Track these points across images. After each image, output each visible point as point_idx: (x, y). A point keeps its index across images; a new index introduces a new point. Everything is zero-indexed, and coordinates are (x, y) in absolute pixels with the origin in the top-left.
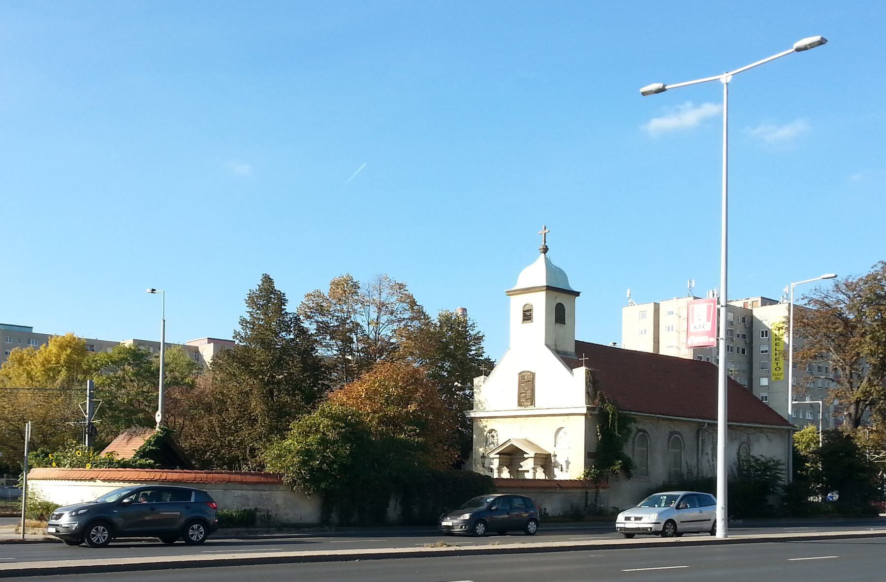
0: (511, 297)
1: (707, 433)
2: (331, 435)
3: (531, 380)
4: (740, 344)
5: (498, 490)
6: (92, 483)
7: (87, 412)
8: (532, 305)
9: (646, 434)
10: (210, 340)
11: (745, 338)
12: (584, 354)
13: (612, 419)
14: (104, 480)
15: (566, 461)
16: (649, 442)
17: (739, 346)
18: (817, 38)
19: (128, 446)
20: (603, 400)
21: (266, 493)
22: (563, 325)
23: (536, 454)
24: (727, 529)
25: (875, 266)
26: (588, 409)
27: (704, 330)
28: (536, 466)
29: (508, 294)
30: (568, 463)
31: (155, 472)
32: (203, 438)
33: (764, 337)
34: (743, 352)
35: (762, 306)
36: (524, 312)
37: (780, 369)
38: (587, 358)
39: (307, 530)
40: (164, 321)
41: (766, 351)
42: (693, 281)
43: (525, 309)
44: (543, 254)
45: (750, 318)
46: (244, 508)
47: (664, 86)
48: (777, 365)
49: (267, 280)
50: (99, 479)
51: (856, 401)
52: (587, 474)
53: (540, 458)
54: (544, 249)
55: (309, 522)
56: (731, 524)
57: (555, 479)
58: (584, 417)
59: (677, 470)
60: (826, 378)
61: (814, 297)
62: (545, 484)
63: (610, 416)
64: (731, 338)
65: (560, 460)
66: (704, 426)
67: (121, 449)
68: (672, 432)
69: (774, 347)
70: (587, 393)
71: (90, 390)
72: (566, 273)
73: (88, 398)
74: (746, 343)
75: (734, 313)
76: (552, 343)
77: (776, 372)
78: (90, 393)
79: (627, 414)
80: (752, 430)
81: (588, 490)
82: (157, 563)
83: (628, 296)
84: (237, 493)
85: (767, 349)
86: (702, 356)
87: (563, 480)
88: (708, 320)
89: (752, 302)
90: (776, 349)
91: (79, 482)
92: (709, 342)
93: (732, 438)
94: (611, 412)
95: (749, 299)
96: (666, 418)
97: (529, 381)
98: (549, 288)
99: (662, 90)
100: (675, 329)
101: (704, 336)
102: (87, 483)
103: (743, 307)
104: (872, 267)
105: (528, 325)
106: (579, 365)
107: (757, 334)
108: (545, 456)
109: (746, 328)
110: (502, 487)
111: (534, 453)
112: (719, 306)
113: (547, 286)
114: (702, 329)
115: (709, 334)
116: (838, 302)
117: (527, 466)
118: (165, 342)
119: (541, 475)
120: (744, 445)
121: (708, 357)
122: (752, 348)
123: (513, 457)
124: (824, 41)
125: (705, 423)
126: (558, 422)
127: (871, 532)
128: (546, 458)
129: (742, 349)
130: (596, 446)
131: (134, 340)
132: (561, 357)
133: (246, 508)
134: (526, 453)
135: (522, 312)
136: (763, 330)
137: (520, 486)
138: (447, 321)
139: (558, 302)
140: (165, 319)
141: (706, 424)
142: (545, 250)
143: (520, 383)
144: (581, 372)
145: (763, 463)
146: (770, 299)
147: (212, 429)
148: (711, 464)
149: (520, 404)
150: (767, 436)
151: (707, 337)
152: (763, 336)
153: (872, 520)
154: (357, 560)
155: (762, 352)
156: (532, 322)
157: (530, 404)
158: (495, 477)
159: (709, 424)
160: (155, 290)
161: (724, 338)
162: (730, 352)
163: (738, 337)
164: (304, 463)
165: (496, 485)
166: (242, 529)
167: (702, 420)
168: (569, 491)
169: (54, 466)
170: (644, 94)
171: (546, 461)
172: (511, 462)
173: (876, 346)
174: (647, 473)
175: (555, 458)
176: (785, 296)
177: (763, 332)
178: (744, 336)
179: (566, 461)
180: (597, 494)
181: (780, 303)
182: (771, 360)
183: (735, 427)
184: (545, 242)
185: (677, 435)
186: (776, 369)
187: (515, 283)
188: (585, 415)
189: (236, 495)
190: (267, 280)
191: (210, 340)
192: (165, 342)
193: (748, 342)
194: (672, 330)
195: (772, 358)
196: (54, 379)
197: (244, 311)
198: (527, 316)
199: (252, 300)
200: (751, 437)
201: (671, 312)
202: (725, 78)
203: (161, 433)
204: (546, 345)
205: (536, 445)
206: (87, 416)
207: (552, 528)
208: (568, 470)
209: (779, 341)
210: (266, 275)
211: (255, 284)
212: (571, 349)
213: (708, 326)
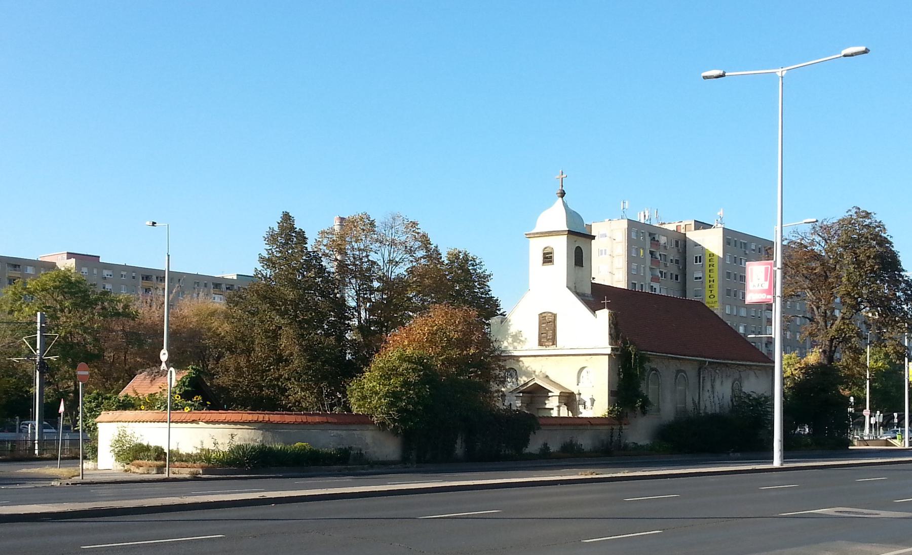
0: (529, 239)
1: (707, 371)
2: (413, 378)
3: (553, 320)
5: (541, 427)
6: (194, 425)
7: (38, 347)
8: (552, 248)
9: (657, 373)
11: (678, 264)
12: (606, 297)
13: (634, 359)
14: (207, 422)
15: (590, 399)
16: (660, 380)
17: (672, 272)
18: (863, 48)
19: (153, 386)
20: (625, 343)
21: (358, 432)
22: (581, 268)
23: (561, 393)
24: (783, 460)
25: (850, 210)
26: (612, 349)
27: (762, 288)
28: (560, 404)
29: (528, 236)
30: (593, 401)
31: (257, 413)
32: (231, 378)
33: (698, 263)
34: (677, 279)
35: (695, 229)
36: (544, 254)
37: (714, 296)
38: (609, 301)
39: (393, 466)
40: (169, 256)
41: (700, 278)
42: (627, 202)
43: (545, 252)
44: (561, 199)
45: (683, 243)
46: (339, 447)
47: (724, 73)
48: (711, 292)
49: (287, 217)
50: (202, 421)
51: (831, 338)
52: (610, 412)
53: (564, 396)
54: (561, 193)
55: (393, 460)
56: (785, 457)
57: (580, 416)
58: (607, 356)
60: (803, 317)
61: (794, 239)
62: (570, 422)
63: (633, 356)
64: (665, 264)
65: (586, 397)
66: (705, 364)
67: (146, 389)
68: (678, 370)
70: (610, 334)
71: (41, 324)
72: (582, 217)
73: (38, 332)
74: (679, 269)
75: (667, 237)
77: (710, 300)
78: (41, 326)
79: (644, 353)
81: (613, 427)
82: (542, 481)
84: (333, 433)
85: (701, 276)
86: (636, 282)
87: (591, 418)
88: (766, 280)
89: (686, 225)
90: (710, 275)
91: (179, 424)
92: (766, 298)
93: (727, 376)
94: (634, 353)
95: (682, 222)
96: (675, 358)
97: (550, 322)
98: (570, 233)
99: (723, 76)
100: (608, 252)
101: (762, 293)
102: (189, 425)
103: (676, 230)
104: (847, 212)
105: (548, 267)
106: (602, 307)
107: (690, 259)
108: (567, 395)
109: (680, 252)
110: (544, 425)
111: (560, 391)
112: (775, 269)
113: (568, 230)
114: (760, 288)
115: (768, 292)
116: (812, 243)
117: (551, 404)
118: (170, 270)
119: (564, 412)
120: (737, 382)
121: (642, 283)
122: (686, 275)
123: (534, 395)
124: (867, 51)
125: (706, 361)
127: (881, 461)
128: (568, 397)
129: (676, 275)
130: (617, 385)
132: (582, 299)
133: (341, 446)
134: (551, 392)
135: (542, 255)
136: (696, 255)
137: (559, 423)
138: (455, 257)
139: (577, 246)
140: (169, 254)
141: (707, 363)
142: (563, 194)
143: (540, 324)
144: (604, 315)
145: (754, 398)
146: (703, 223)
147: (238, 368)
148: (712, 401)
149: (541, 344)
150: (755, 374)
151: (765, 295)
152: (696, 262)
153: (697, 458)
154: (273, 505)
155: (696, 278)
156: (553, 264)
157: (551, 343)
158: (553, 416)
159: (709, 362)
160: (155, 223)
161: (780, 296)
162: (663, 278)
163: (672, 262)
164: (391, 405)
165: (540, 423)
166: (340, 466)
167: (703, 359)
168: (598, 427)
169: (143, 409)
170: (705, 78)
171: (569, 399)
172: (531, 400)
173: (852, 287)
174: (659, 410)
175: (580, 396)
176: (719, 220)
177: (696, 257)
178: (677, 262)
179: (590, 399)
180: (620, 430)
181: (714, 227)
182: (705, 288)
183: (729, 365)
184: (562, 186)
185: (683, 374)
186: (710, 297)
187: (534, 226)
189: (332, 435)
190: (287, 217)
191: (70, 255)
192: (170, 270)
193: (681, 268)
194: (605, 254)
195: (706, 286)
197: (263, 249)
198: (548, 258)
199: (272, 238)
200: (743, 374)
201: (603, 234)
202: (779, 72)
203: (194, 374)
204: (567, 287)
205: (557, 384)
206: (38, 352)
207: (589, 463)
208: (593, 408)
209: (713, 268)
210: (286, 212)
211: (273, 221)
212: (588, 291)
213: (766, 286)
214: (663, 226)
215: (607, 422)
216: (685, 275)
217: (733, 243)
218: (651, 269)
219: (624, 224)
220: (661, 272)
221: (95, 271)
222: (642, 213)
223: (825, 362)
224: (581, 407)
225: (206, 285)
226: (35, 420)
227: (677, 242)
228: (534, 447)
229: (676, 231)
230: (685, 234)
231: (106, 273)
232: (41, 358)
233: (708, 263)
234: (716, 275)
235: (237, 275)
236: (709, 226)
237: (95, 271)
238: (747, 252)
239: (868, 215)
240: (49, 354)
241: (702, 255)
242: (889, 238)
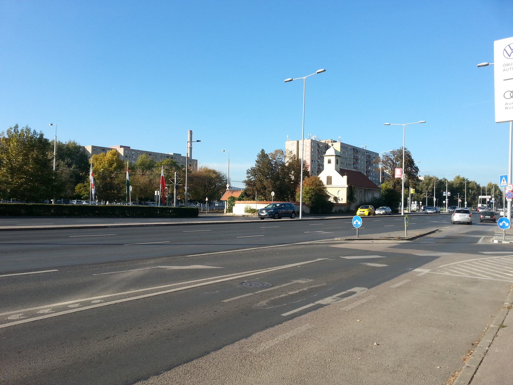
7: (175, 181)
10: (121, 147)
30: (342, 199)
36: (328, 161)
42: (310, 134)
49: (263, 150)
65: (340, 198)
70: (347, 182)
71: (176, 175)
73: (175, 178)
76: (336, 169)
80: (374, 190)
83: (287, 137)
98: (336, 156)
102: (259, 204)
105: (329, 164)
126: (339, 189)
131: (92, 146)
143: (327, 179)
144: (345, 177)
164: (310, 200)
171: (336, 199)
180: (350, 206)
188: (347, 188)
190: (263, 150)
191: (121, 147)
196: (112, 166)
198: (329, 162)
199: (259, 156)
202: (404, 125)
206: (175, 183)
211: (259, 152)
214: (320, 141)
215: (347, 205)
217: (343, 147)
218: (318, 155)
219: (310, 141)
220: (320, 156)
221: (130, 152)
222: (313, 137)
223: (393, 189)
224: (339, 201)
225: (164, 157)
226: (506, 207)
227: (325, 146)
228: (334, 210)
229: (325, 143)
230: (328, 144)
231: (133, 152)
232: (176, 185)
235: (174, 153)
236: (336, 142)
237: (130, 152)
238: (348, 150)
240: (179, 184)
242: (411, 155)
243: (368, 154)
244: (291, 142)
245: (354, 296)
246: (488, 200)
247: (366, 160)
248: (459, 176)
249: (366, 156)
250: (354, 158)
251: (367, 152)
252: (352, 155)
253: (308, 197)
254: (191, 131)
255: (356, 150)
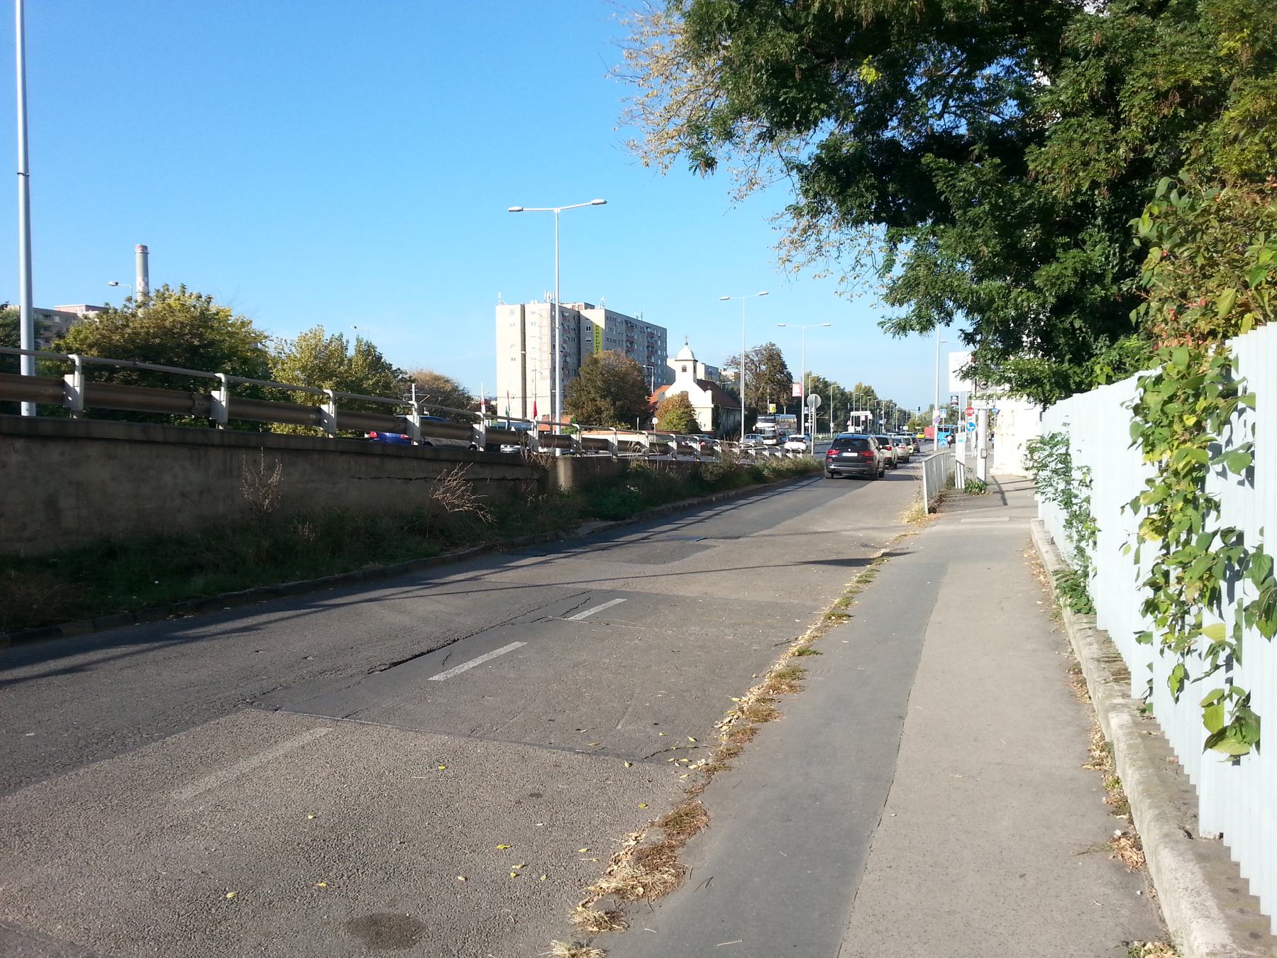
4: (573, 334)
18: (603, 201)
49: (1226, 479)
59: (283, 582)
69: (595, 338)
118: (35, 305)
144: (709, 393)
192: (35, 305)
198: (684, 370)
202: (557, 210)
216: (579, 339)
229: (572, 309)
233: (595, 331)
234: (600, 339)
239: (774, 345)
241: (590, 326)
243: (649, 330)
244: (507, 308)
245: (707, 552)
246: (863, 418)
247: (646, 344)
248: (774, 359)
249: (646, 334)
250: (627, 341)
251: (649, 326)
252: (625, 336)
253: (683, 423)
254: (144, 248)
255: (630, 324)
